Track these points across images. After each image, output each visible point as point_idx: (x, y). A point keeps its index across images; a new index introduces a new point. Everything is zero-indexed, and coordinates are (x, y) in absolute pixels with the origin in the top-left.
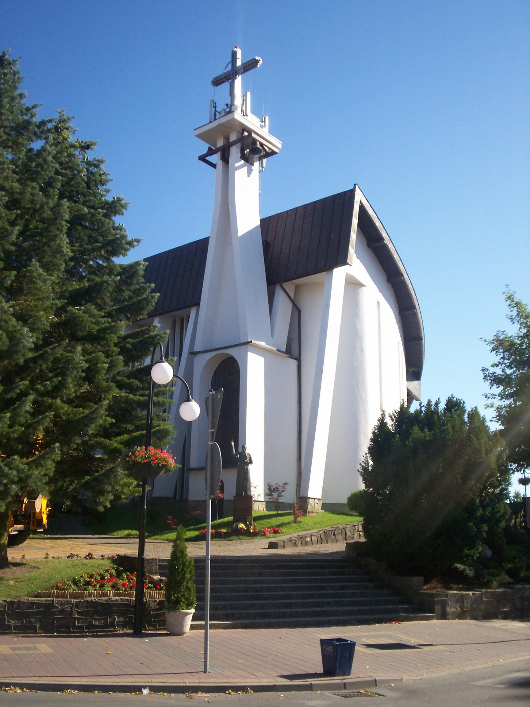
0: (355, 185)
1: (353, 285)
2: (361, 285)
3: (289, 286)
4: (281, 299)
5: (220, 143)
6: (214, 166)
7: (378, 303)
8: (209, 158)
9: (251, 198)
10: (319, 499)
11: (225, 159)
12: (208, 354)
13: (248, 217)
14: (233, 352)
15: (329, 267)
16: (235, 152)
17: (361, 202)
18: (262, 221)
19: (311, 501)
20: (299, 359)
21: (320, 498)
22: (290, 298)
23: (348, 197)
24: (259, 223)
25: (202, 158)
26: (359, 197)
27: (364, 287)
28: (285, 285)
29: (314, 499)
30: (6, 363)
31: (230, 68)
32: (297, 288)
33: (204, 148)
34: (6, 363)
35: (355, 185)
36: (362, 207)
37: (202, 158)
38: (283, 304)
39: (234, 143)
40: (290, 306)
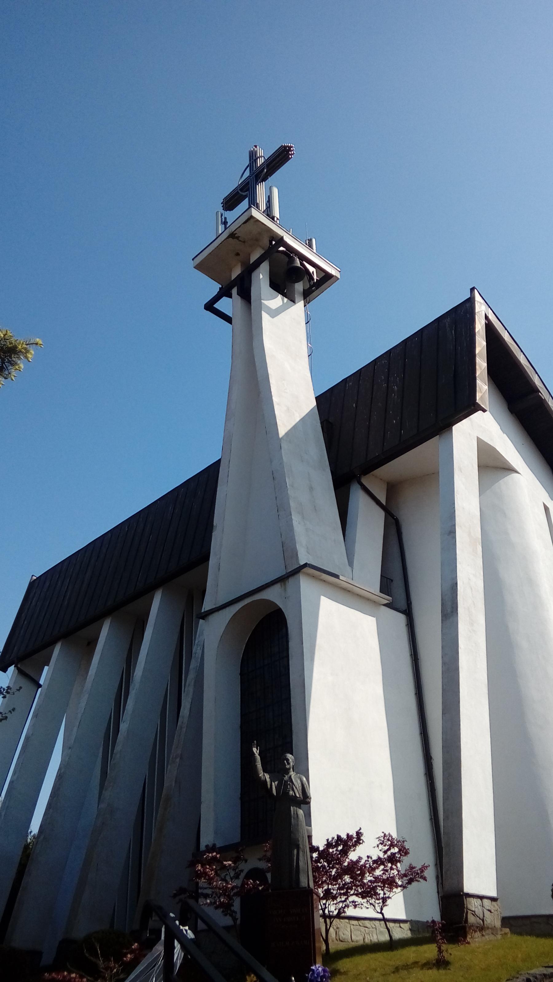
0: (472, 290)
1: (492, 466)
2: (509, 469)
3: (375, 482)
4: (360, 502)
5: (236, 272)
6: (228, 319)
7: (546, 509)
8: (220, 305)
9: (293, 358)
10: (493, 899)
11: (246, 295)
12: (228, 609)
13: (293, 396)
14: (272, 595)
15: (443, 425)
16: (262, 277)
17: (486, 317)
18: (317, 398)
19: (473, 905)
20: (408, 612)
21: (493, 893)
22: (378, 502)
23: (464, 312)
24: (315, 403)
25: (210, 307)
26: (481, 308)
27: (515, 475)
28: (365, 481)
29: (481, 898)
30: (129, 956)
31: (247, 174)
32: (393, 488)
33: (214, 288)
34: (129, 956)
35: (472, 290)
36: (489, 327)
37: (210, 307)
38: (369, 522)
39: (257, 264)
40: (379, 516)
